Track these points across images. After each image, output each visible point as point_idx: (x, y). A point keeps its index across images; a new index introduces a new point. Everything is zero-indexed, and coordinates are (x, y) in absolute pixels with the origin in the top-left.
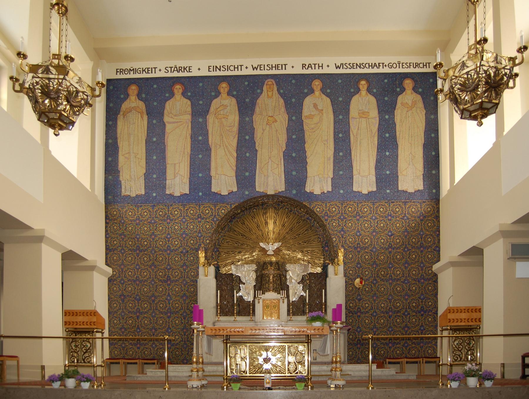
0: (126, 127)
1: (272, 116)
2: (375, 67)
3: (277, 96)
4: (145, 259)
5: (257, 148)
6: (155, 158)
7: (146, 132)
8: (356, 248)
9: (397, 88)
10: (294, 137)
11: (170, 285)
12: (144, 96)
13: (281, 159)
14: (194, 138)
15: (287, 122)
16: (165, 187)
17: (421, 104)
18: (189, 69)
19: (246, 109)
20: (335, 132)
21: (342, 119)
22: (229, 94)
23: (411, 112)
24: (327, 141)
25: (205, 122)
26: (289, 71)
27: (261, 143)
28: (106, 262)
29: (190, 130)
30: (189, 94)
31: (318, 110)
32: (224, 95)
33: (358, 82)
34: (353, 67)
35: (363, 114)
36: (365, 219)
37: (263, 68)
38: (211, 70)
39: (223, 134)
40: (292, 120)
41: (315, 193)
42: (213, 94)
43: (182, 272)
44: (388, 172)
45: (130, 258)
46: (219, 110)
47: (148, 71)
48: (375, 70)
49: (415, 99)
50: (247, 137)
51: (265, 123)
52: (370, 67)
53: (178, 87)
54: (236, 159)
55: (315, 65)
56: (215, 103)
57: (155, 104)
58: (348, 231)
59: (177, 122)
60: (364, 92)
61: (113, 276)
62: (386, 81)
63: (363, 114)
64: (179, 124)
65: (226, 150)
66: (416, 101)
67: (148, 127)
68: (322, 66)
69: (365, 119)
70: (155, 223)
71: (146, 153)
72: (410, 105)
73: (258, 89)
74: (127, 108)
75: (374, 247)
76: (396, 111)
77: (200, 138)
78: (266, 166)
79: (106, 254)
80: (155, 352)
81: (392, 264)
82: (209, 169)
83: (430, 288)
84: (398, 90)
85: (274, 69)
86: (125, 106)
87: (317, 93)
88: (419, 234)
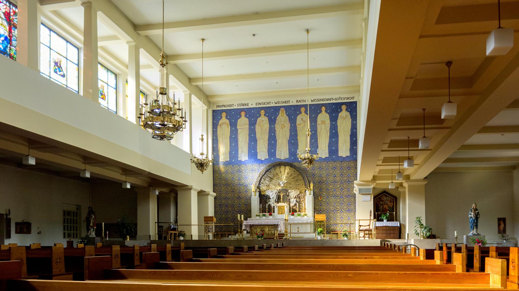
17: (349, 117)
19: (272, 121)
25: (255, 128)
32: (263, 116)
33: (321, 108)
48: (329, 102)
56: (259, 119)
63: (323, 122)
82: (256, 149)
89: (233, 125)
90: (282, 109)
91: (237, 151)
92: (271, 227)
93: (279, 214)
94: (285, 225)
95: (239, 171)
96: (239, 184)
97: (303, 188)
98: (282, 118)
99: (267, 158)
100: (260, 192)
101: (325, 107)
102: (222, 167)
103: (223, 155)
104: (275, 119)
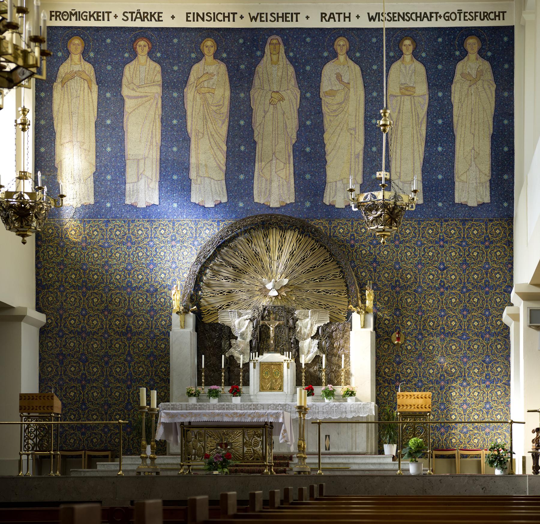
0: (66, 101)
1: (277, 92)
2: (425, 19)
3: (285, 61)
4: (95, 300)
5: (256, 139)
6: (109, 149)
7: (96, 110)
8: (393, 288)
9: (456, 50)
10: (308, 123)
11: (131, 339)
12: (92, 55)
13: (289, 156)
14: (165, 121)
15: (299, 100)
16: (124, 194)
17: (489, 76)
18: (159, 17)
19: (241, 79)
20: (366, 117)
21: (376, 98)
22: (216, 56)
23: (475, 86)
24: (355, 129)
25: (182, 98)
26: (302, 23)
27: (261, 132)
28: (37, 304)
29: (160, 110)
30: (159, 55)
31: (342, 80)
32: (209, 58)
33: (399, 42)
34: (393, 19)
35: (407, 90)
36: (407, 244)
37: (264, 19)
38: (191, 18)
39: (208, 117)
40: (306, 98)
41: (337, 206)
42: (193, 55)
43: (148, 320)
44: (440, 177)
45: (73, 299)
46: (201, 80)
47: (98, 16)
48: (425, 24)
49: (481, 68)
50: (242, 123)
51: (267, 102)
52: (419, 19)
53: (142, 43)
54: (225, 155)
55: (339, 14)
56: (197, 70)
57: (109, 68)
58: (383, 262)
59: (141, 97)
60: (408, 57)
61: (47, 325)
62: (440, 40)
63: (407, 90)
64: (144, 99)
65: (212, 140)
66: (482, 71)
67: (99, 103)
68: (349, 17)
69: (409, 98)
70: (109, 247)
71: (97, 142)
72: (474, 76)
73: (257, 50)
74: (67, 74)
75: (420, 286)
76: (453, 87)
77: (175, 122)
78: (269, 164)
79: (38, 293)
80: (108, 440)
81: (444, 311)
82: (188, 169)
83: (499, 346)
84: (457, 53)
85: (280, 19)
86: (64, 69)
87: (342, 58)
88: (484, 267)
89: (109, 85)
90: (275, 39)
91: (123, 173)
92: (251, 432)
93: (262, 388)
94: (301, 426)
95: (129, 240)
96: (129, 285)
97: (342, 303)
98: (275, 71)
99: (224, 200)
100: (199, 316)
101: (414, 40)
102: (71, 226)
103: (75, 184)
104: (251, 73)
